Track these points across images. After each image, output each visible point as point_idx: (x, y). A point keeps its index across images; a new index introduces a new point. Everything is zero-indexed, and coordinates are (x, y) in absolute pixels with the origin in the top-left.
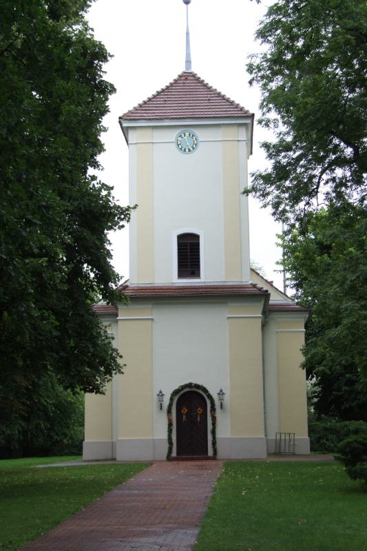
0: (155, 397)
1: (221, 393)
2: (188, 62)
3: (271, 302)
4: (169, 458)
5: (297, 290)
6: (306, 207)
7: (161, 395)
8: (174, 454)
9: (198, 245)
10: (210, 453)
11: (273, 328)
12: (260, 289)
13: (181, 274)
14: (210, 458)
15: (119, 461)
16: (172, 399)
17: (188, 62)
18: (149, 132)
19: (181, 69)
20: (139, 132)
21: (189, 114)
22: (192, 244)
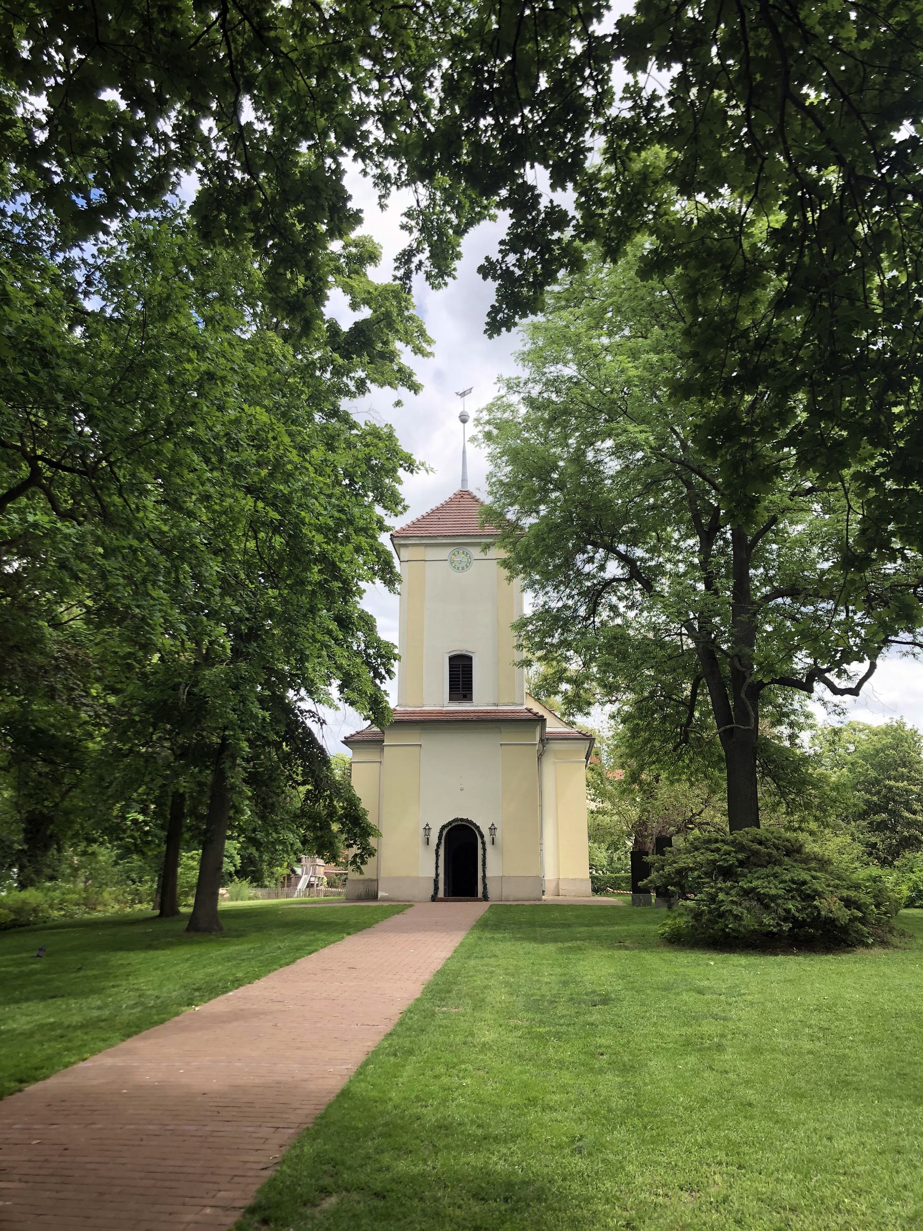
0: (422, 832)
1: (492, 829)
2: (464, 480)
3: (548, 730)
4: (434, 898)
5: (374, 65)
6: (781, 346)
7: (427, 829)
8: (441, 894)
9: (470, 667)
10: (480, 895)
11: (550, 767)
12: (535, 714)
13: (453, 697)
14: (480, 900)
15: (384, 900)
16: (440, 838)
17: (464, 480)
18: (422, 549)
19: (457, 487)
20: (410, 549)
21: (462, 532)
22: (464, 666)
